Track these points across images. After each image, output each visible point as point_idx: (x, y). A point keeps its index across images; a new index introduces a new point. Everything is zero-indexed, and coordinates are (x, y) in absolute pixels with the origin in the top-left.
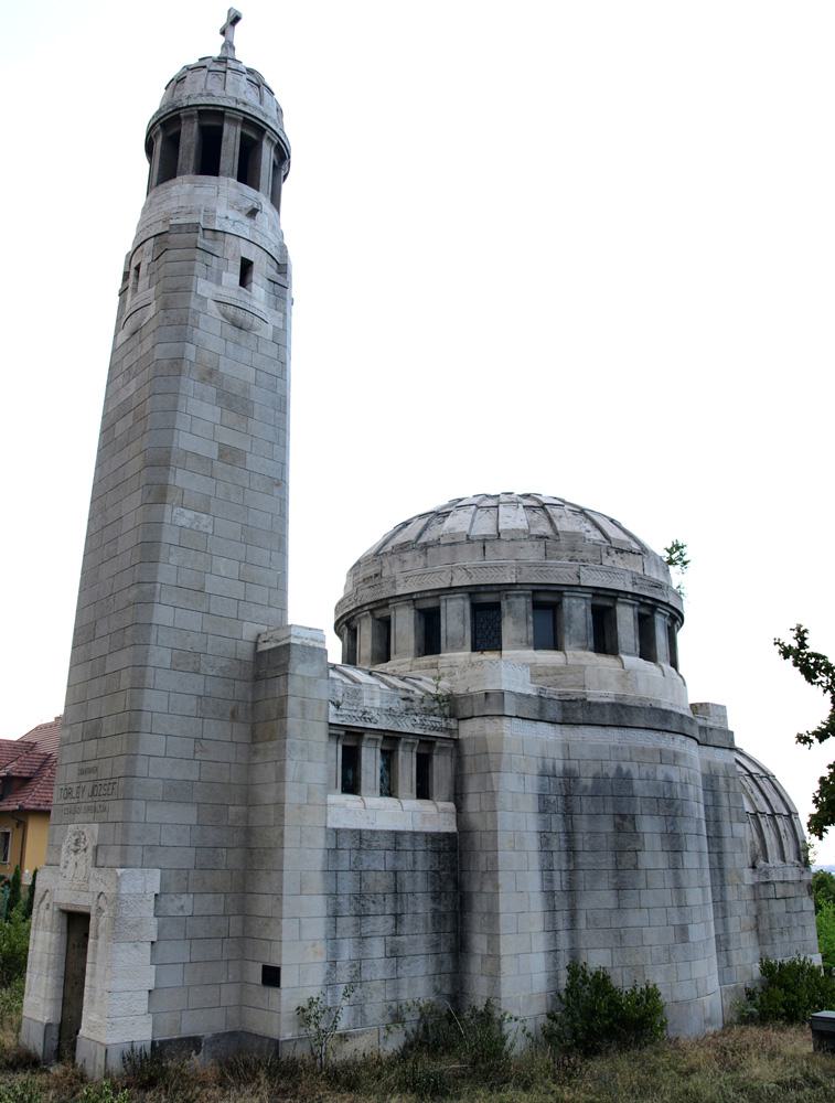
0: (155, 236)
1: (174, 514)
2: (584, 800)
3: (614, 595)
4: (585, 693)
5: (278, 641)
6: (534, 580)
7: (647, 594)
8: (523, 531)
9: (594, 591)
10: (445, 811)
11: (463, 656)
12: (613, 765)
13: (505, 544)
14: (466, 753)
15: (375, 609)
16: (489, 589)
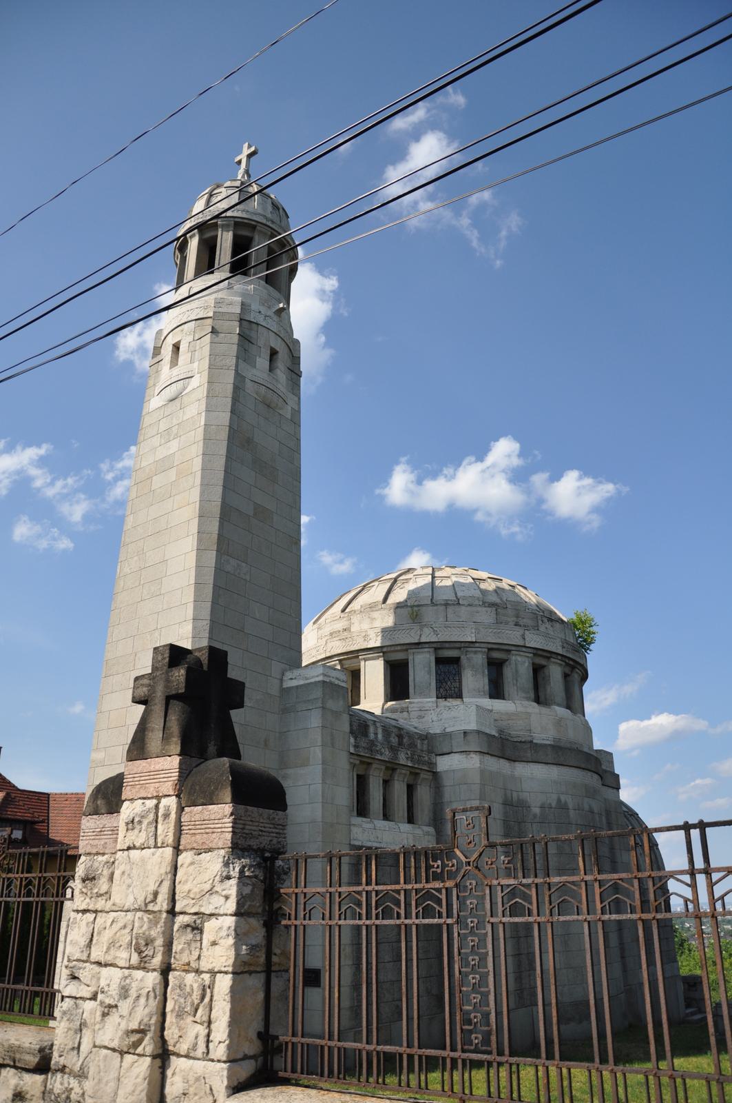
0: (196, 320)
1: (222, 561)
2: (534, 825)
3: (549, 655)
4: (532, 736)
5: (307, 679)
7: (571, 656)
8: (478, 598)
9: (535, 652)
10: (428, 833)
11: (430, 701)
12: (555, 797)
13: (463, 608)
14: (445, 784)
15: (344, 659)
16: (452, 645)
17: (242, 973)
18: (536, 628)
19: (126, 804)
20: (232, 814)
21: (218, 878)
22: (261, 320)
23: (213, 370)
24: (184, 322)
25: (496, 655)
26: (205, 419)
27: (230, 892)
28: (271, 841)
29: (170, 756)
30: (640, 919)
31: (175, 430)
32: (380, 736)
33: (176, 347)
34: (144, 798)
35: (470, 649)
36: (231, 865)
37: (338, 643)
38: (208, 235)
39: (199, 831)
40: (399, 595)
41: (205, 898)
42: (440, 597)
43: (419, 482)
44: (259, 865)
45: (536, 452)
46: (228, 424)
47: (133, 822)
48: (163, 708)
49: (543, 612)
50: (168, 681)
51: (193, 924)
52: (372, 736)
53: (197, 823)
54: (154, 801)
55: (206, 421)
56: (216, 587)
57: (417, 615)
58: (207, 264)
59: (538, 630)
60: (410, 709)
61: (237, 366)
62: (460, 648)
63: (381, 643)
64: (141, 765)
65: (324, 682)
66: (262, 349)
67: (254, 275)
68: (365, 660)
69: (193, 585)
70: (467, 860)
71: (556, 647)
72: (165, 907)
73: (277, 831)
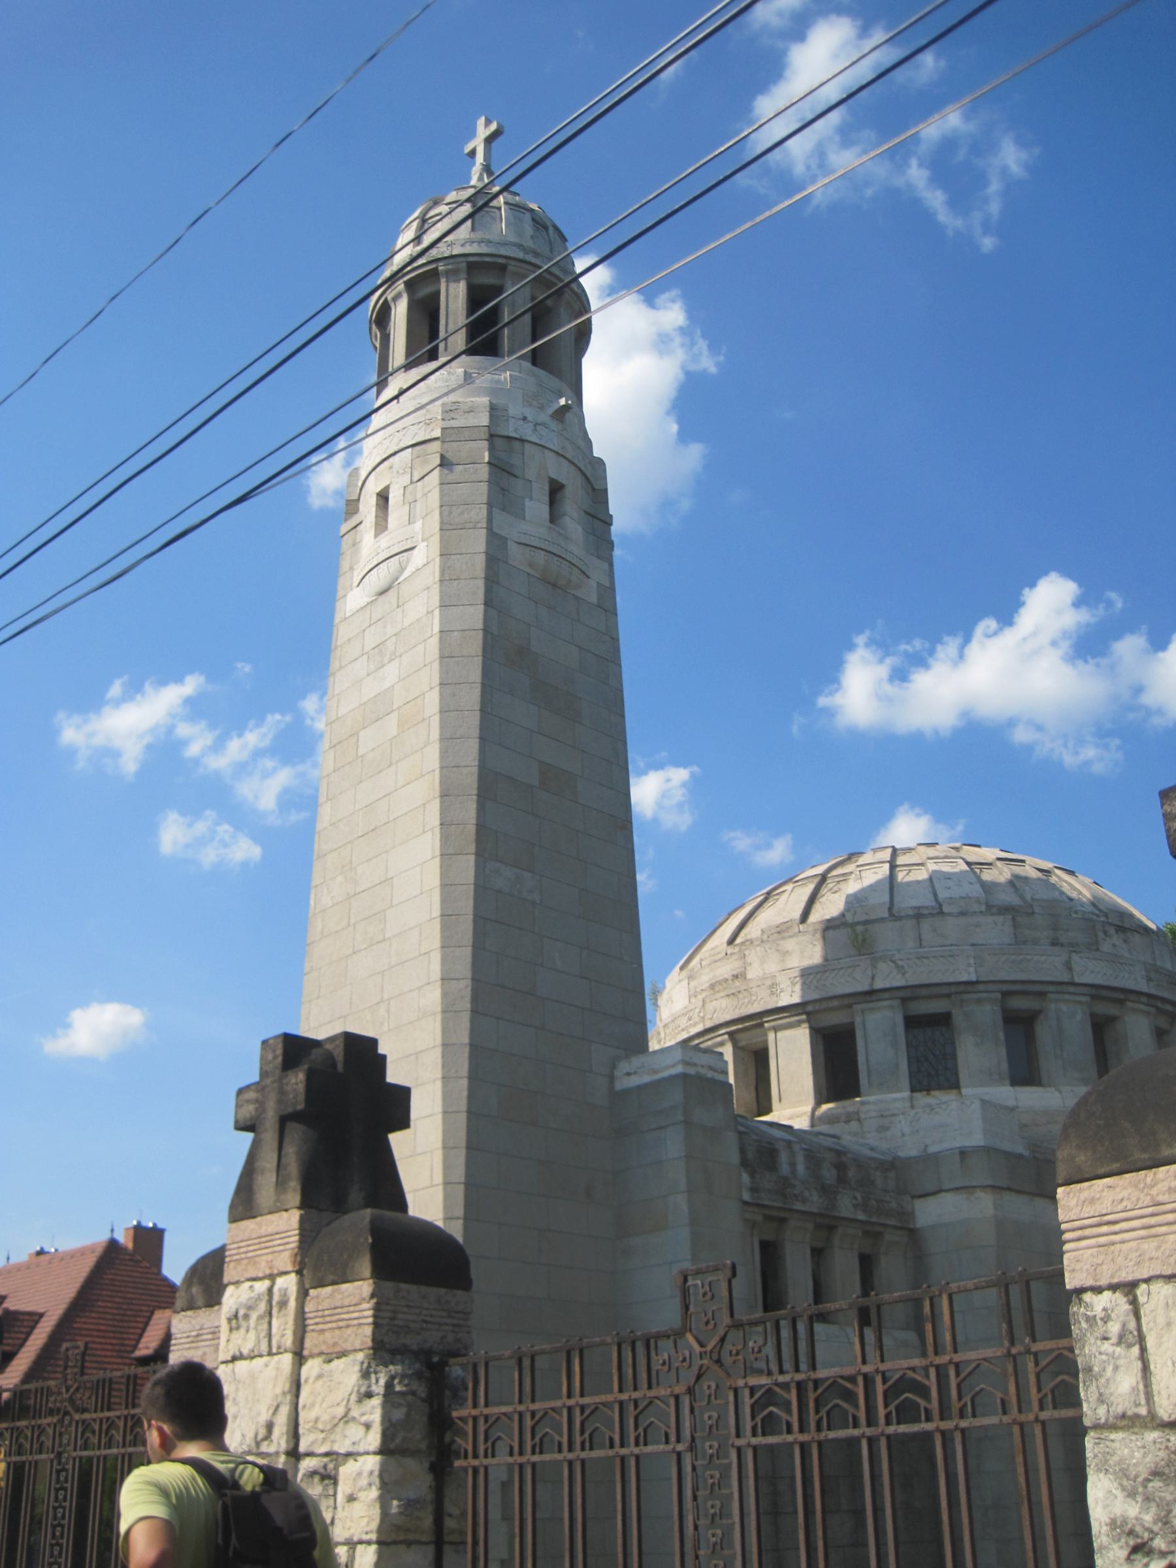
0: (413, 446)
3: (1122, 996)
5: (655, 1072)
6: (1003, 975)
7: (1166, 995)
8: (978, 901)
9: (1093, 991)
11: (898, 1097)
17: (395, 1543)
18: (1093, 946)
19: (230, 1290)
20: (373, 1296)
21: (354, 1397)
22: (527, 432)
23: (448, 533)
24: (392, 451)
25: (1019, 1003)
26: (441, 621)
27: (372, 1417)
28: (444, 1337)
29: (286, 1210)
30: (938, 1429)
31: (390, 645)
32: (801, 1169)
33: (383, 498)
34: (254, 1279)
35: (966, 996)
36: (373, 1376)
37: (724, 1003)
38: (425, 291)
39: (330, 1325)
40: (831, 906)
41: (338, 1430)
42: (906, 903)
43: (900, 676)
44: (418, 1375)
45: (1113, 595)
46: (481, 626)
47: (236, 1316)
48: (276, 1136)
49: (1106, 916)
50: (282, 1092)
51: (322, 1471)
52: (785, 1169)
53: (327, 1312)
54: (267, 1283)
55: (441, 624)
56: (479, 919)
57: (864, 940)
58: (425, 344)
59: (1098, 949)
60: (862, 1116)
61: (490, 520)
62: (948, 996)
63: (802, 996)
64: (249, 1226)
65: (685, 1076)
66: (534, 485)
67: (511, 353)
68: (776, 1029)
69: (438, 920)
70: (703, 1350)
71: (1134, 980)
72: (284, 1446)
73: (455, 1322)
